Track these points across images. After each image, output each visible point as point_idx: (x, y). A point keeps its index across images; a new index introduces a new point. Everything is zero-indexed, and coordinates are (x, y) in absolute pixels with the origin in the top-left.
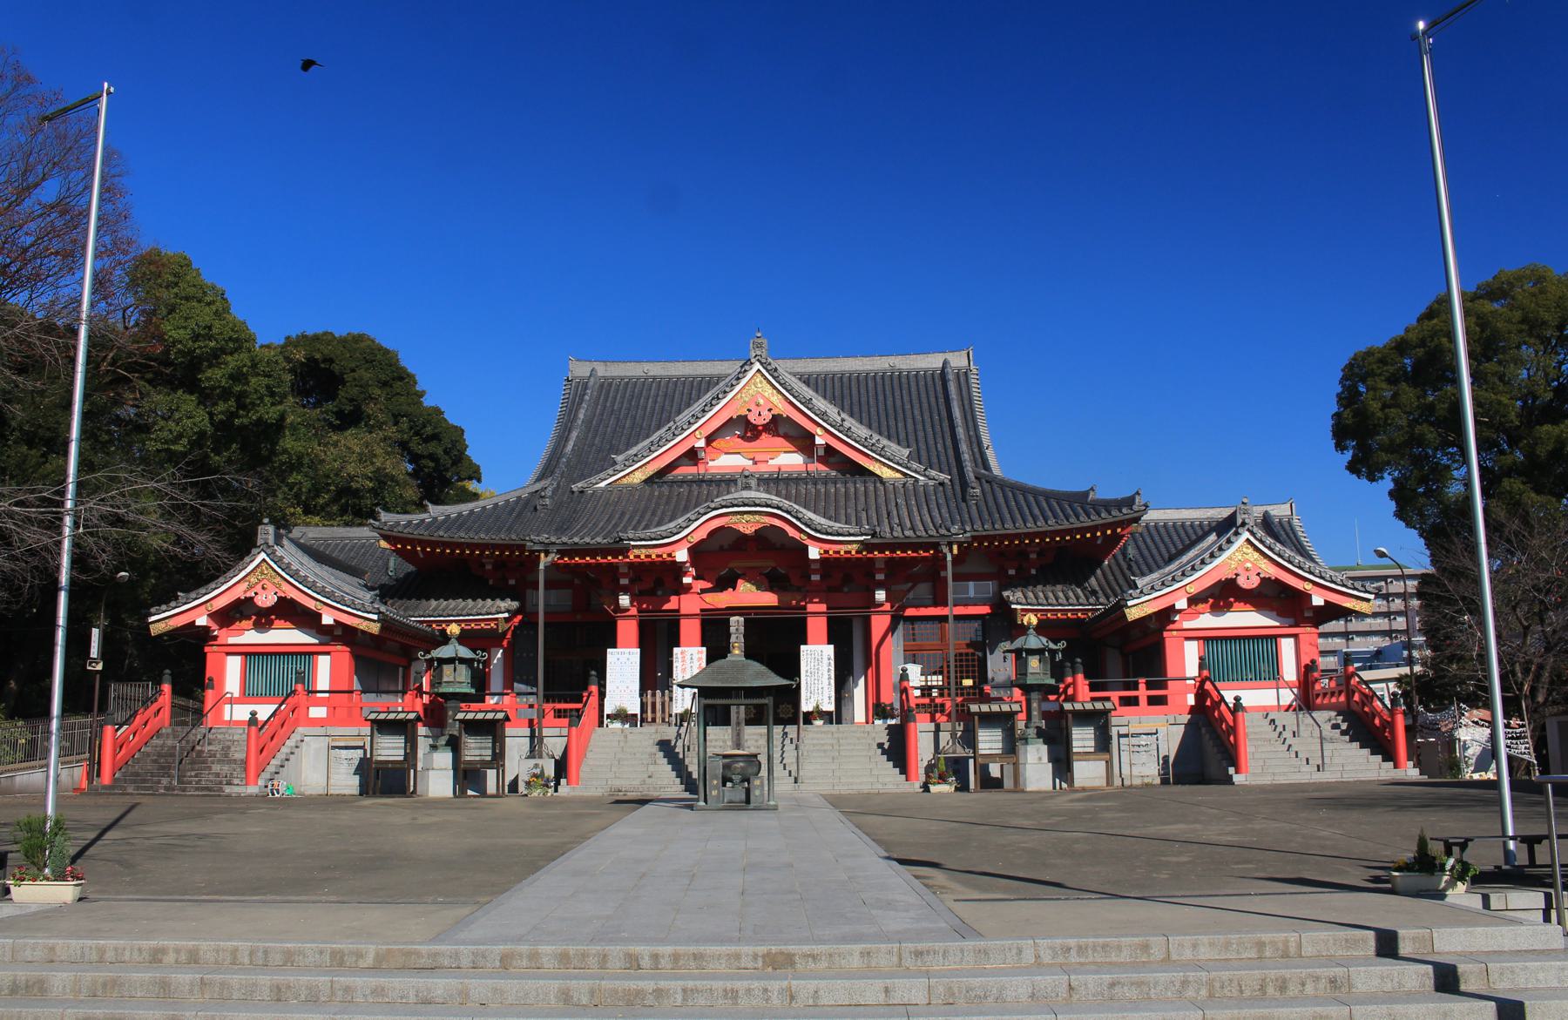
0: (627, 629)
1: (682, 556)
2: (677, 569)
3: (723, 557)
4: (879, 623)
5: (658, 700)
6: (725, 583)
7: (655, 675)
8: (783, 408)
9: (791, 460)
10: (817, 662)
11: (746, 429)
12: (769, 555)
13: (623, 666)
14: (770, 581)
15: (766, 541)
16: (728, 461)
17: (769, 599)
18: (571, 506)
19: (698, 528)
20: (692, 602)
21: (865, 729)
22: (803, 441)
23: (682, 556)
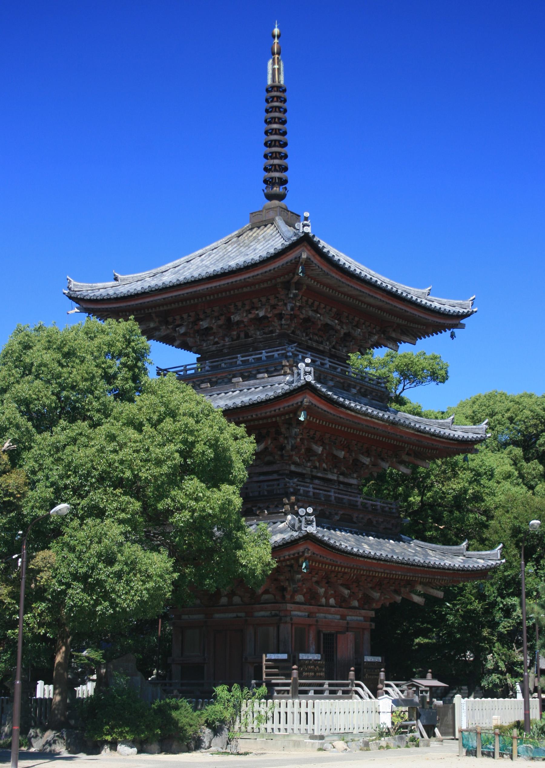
5: (296, 709)
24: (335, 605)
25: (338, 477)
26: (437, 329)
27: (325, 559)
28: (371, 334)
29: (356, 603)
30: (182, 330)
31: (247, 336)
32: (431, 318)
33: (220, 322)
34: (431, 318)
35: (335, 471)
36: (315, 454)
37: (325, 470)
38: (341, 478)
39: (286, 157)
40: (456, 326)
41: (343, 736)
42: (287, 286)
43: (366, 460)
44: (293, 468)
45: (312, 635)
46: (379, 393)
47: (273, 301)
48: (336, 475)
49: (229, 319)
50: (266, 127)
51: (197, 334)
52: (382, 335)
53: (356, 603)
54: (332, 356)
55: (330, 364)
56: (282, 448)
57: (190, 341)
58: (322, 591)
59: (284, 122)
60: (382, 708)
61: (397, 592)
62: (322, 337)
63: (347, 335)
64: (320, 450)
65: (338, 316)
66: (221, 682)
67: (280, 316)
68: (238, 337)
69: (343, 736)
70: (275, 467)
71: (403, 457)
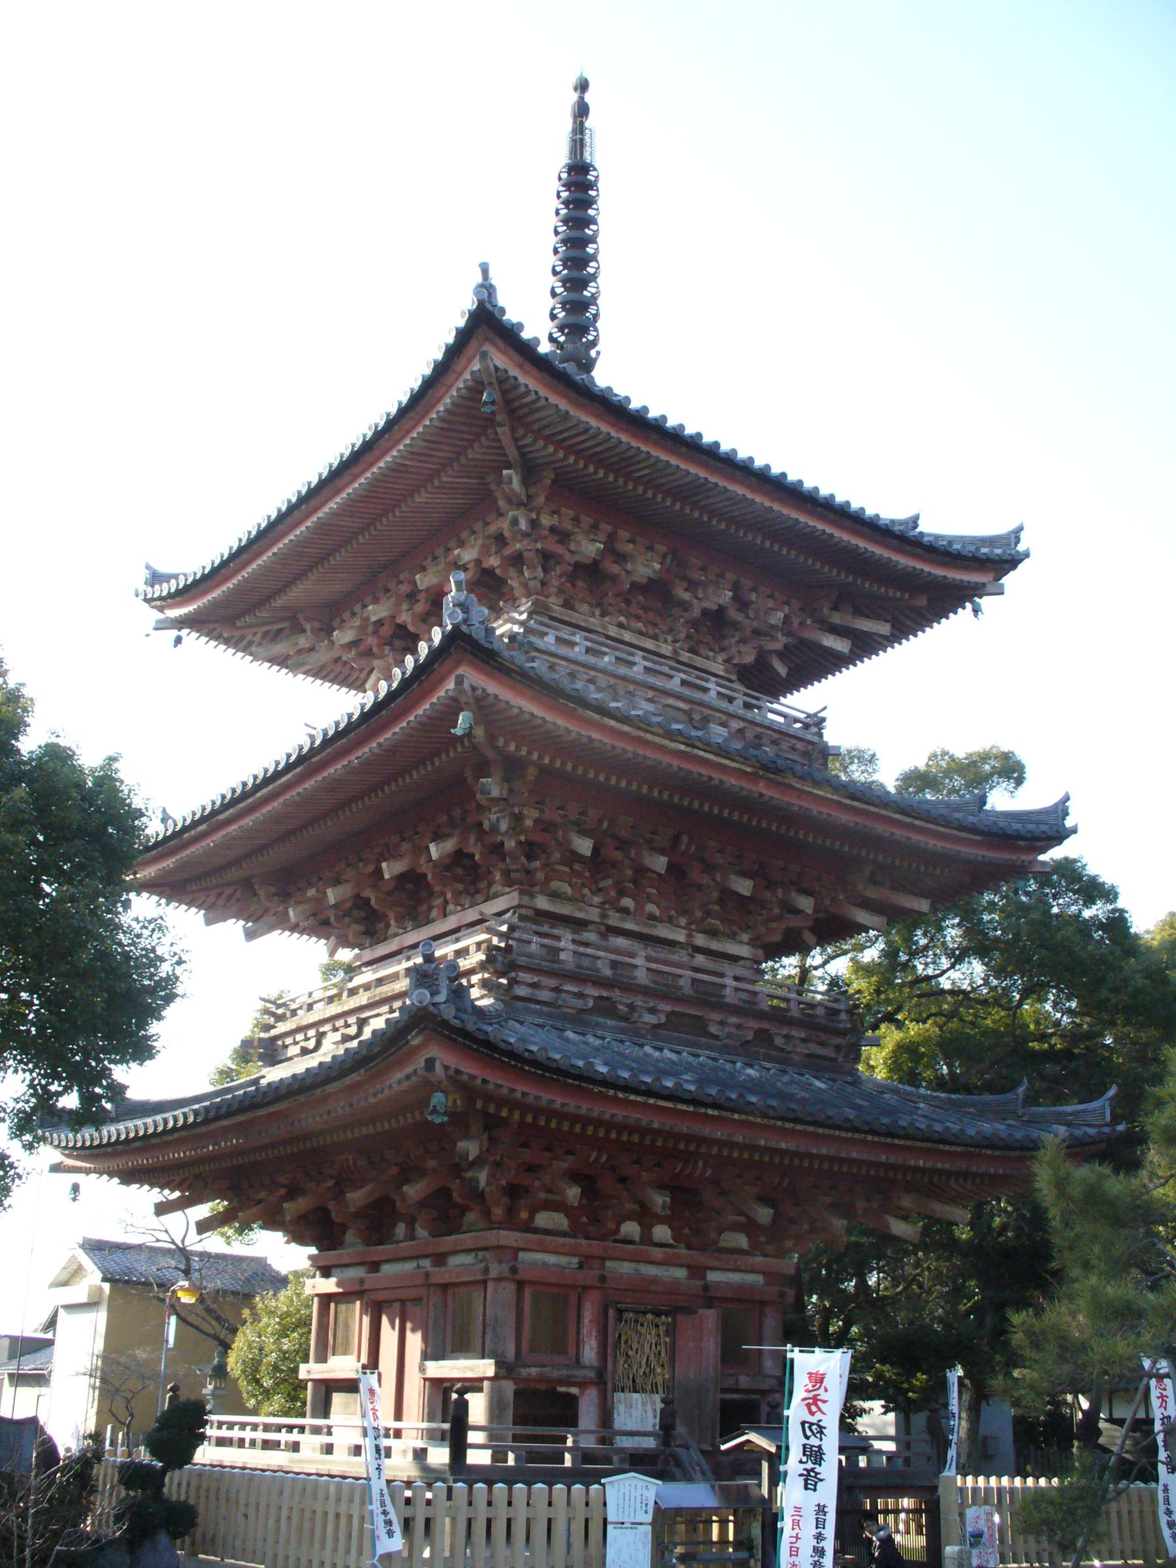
24: (671, 1242)
25: (689, 936)
27: (386, 1092)
35: (683, 921)
37: (652, 917)
38: (700, 940)
41: (492, 1556)
48: (685, 931)
51: (387, 648)
52: (809, 622)
55: (719, 689)
62: (655, 625)
69: (492, 1556)
71: (860, 887)
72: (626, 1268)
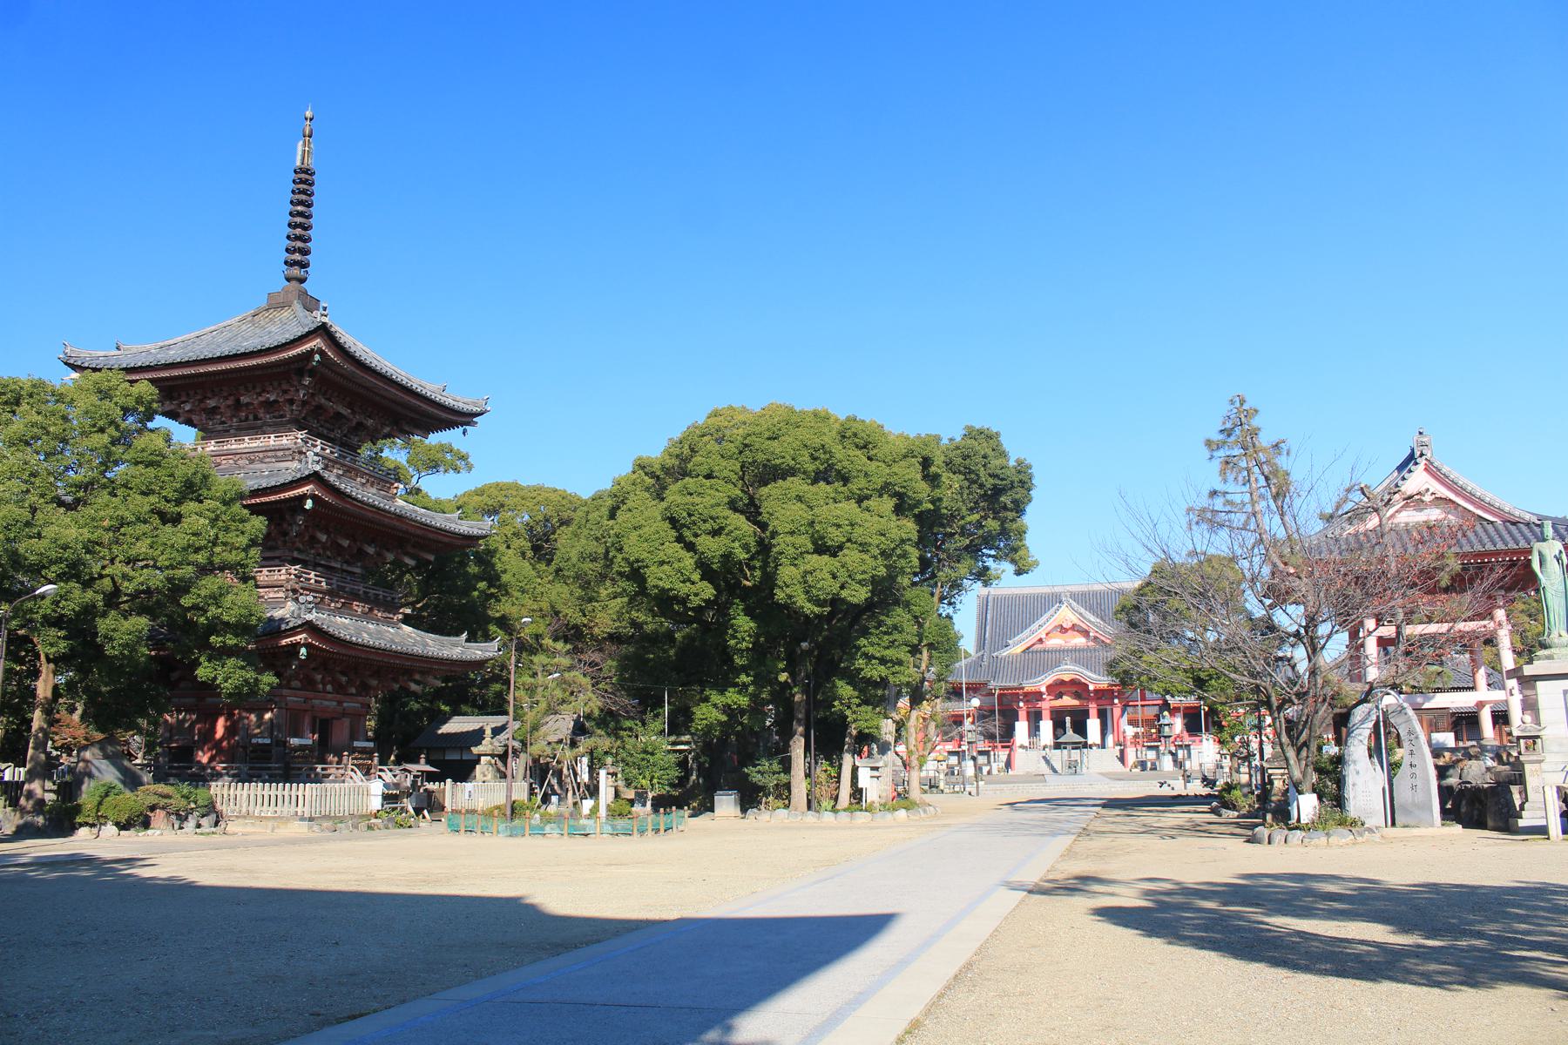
0: (1022, 714)
1: (1043, 689)
2: (1041, 694)
3: (1058, 689)
4: (1117, 711)
5: (286, 793)
6: (1060, 696)
7: (1034, 730)
8: (1076, 621)
9: (1080, 641)
10: (1093, 725)
11: (1063, 630)
12: (1077, 688)
13: (1021, 727)
14: (1077, 696)
15: (1073, 682)
16: (1056, 642)
17: (1076, 702)
18: (997, 666)
19: (1049, 679)
20: (1047, 705)
21: (1112, 750)
22: (1086, 633)
23: (1043, 689)
26: (450, 425)
28: (383, 425)
29: (353, 691)
30: (188, 407)
31: (256, 418)
32: (444, 415)
33: (229, 402)
34: (444, 415)
36: (319, 542)
38: (345, 567)
39: (309, 240)
40: (468, 424)
42: (301, 373)
43: (371, 550)
44: (296, 554)
45: (307, 721)
46: (387, 478)
47: (285, 387)
49: (238, 400)
50: (293, 186)
53: (353, 691)
54: (342, 445)
56: (285, 534)
57: (195, 418)
58: (319, 677)
59: (310, 206)
60: (370, 791)
61: (395, 680)
63: (360, 425)
64: (324, 538)
65: (350, 406)
66: (387, 430)
67: (291, 402)
68: (247, 419)
70: (277, 553)
72: (317, 702)
